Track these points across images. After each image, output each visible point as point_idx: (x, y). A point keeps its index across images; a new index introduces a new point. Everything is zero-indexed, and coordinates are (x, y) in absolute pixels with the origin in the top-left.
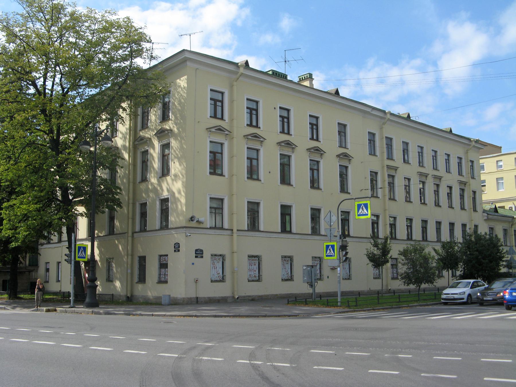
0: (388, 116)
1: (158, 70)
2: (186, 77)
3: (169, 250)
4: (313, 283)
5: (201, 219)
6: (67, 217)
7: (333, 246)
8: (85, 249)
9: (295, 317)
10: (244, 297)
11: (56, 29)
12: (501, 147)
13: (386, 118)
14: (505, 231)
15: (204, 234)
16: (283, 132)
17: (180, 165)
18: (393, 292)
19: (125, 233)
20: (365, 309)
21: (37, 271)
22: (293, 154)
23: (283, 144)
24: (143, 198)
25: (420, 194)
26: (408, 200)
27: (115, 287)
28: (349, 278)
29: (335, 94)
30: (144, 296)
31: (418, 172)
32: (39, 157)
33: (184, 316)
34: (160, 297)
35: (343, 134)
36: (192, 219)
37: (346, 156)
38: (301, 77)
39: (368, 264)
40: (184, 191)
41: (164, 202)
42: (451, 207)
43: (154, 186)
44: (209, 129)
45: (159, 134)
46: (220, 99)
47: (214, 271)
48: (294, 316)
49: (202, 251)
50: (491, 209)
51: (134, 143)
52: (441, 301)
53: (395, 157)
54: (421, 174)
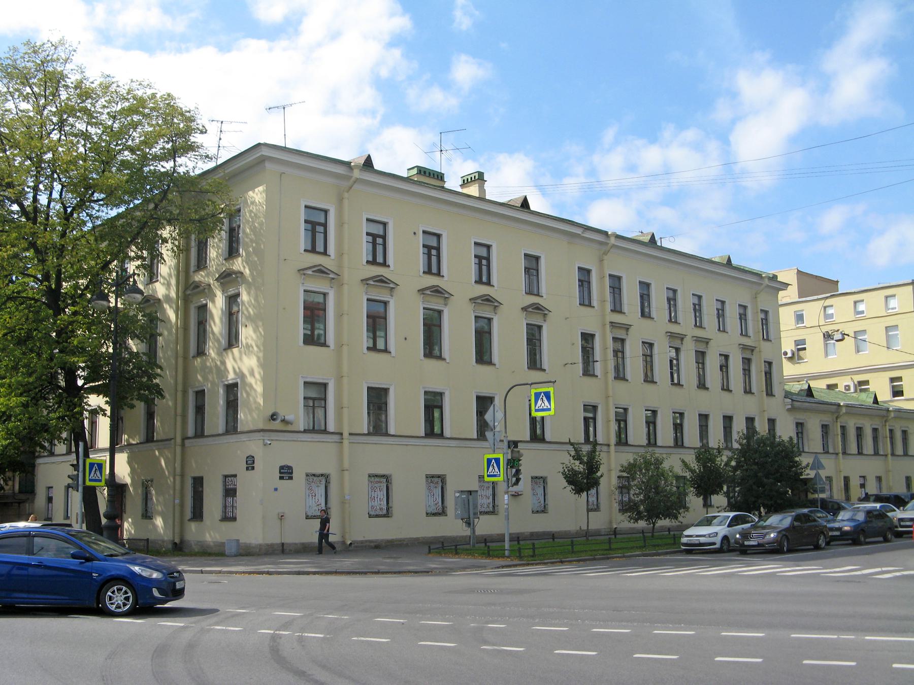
0: (613, 241)
1: (217, 177)
2: (261, 188)
3: (239, 468)
4: (471, 520)
5: (289, 417)
6: (72, 415)
7: (497, 461)
8: (100, 466)
9: (425, 574)
10: (362, 542)
11: (54, 109)
12: (837, 282)
13: (608, 244)
14: (825, 428)
15: (293, 441)
16: (428, 272)
17: (255, 331)
18: (516, 539)
19: (171, 439)
20: (546, 561)
21: (33, 501)
22: (445, 308)
23: (428, 292)
24: (199, 381)
25: (671, 368)
26: (649, 379)
27: (155, 526)
28: (544, 510)
29: (522, 206)
30: (201, 542)
31: (666, 332)
32: (27, 319)
33: (250, 573)
34: (222, 543)
35: (535, 272)
36: (273, 417)
37: (538, 308)
38: (465, 178)
39: (565, 488)
40: (260, 373)
41: (232, 389)
42: (726, 388)
43: (216, 363)
44: (302, 271)
45: (223, 278)
46: (323, 221)
47: (311, 500)
48: (425, 572)
49: (290, 468)
50: (801, 390)
51: (184, 292)
52: (680, 547)
53: (625, 308)
54: (672, 336)
